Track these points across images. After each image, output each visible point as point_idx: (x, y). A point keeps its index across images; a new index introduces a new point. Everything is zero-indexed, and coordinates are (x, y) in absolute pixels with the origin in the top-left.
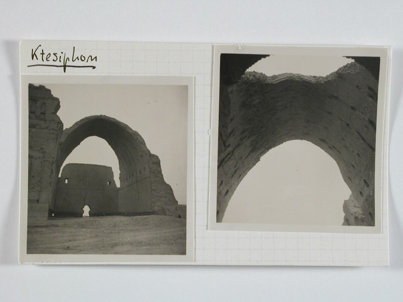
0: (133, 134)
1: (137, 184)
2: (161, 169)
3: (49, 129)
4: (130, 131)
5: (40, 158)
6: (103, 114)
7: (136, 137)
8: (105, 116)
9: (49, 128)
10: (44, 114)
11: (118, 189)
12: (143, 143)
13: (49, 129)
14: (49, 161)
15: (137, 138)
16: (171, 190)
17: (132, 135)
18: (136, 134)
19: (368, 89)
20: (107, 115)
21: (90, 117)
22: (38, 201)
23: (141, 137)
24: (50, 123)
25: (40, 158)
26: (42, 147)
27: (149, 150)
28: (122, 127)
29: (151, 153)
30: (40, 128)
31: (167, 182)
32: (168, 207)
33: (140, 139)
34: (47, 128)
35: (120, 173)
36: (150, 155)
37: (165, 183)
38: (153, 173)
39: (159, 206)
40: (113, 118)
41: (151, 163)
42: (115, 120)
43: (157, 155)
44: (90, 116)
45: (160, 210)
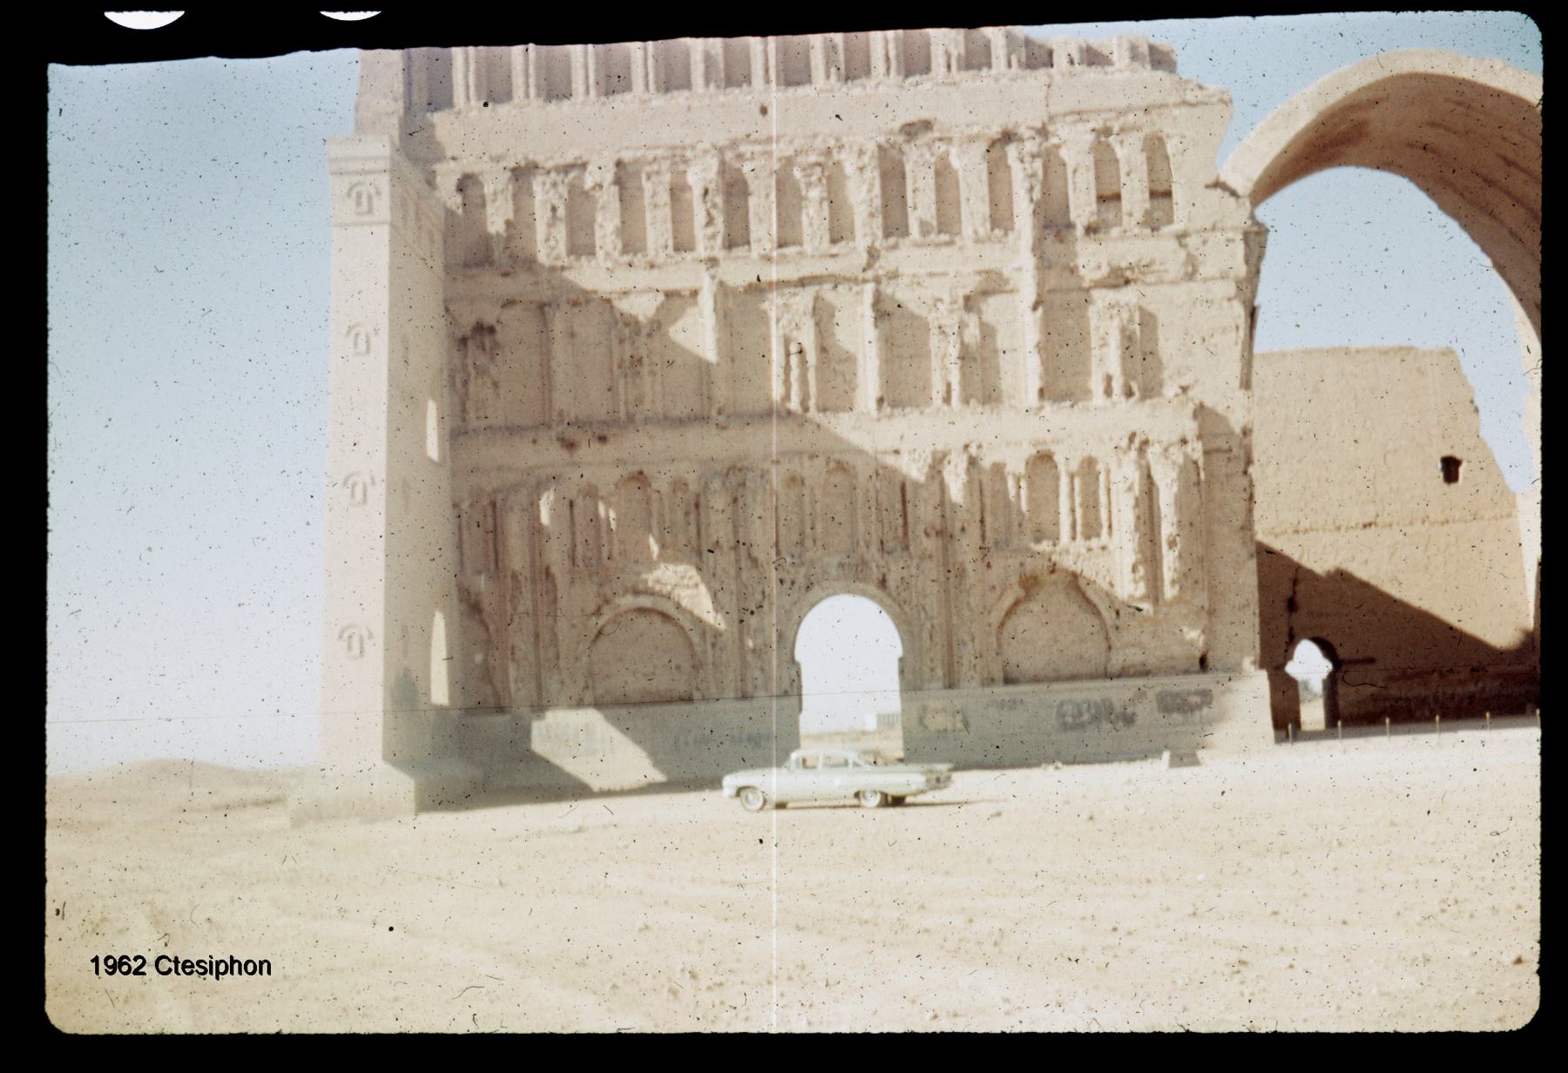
3: (1205, 280)
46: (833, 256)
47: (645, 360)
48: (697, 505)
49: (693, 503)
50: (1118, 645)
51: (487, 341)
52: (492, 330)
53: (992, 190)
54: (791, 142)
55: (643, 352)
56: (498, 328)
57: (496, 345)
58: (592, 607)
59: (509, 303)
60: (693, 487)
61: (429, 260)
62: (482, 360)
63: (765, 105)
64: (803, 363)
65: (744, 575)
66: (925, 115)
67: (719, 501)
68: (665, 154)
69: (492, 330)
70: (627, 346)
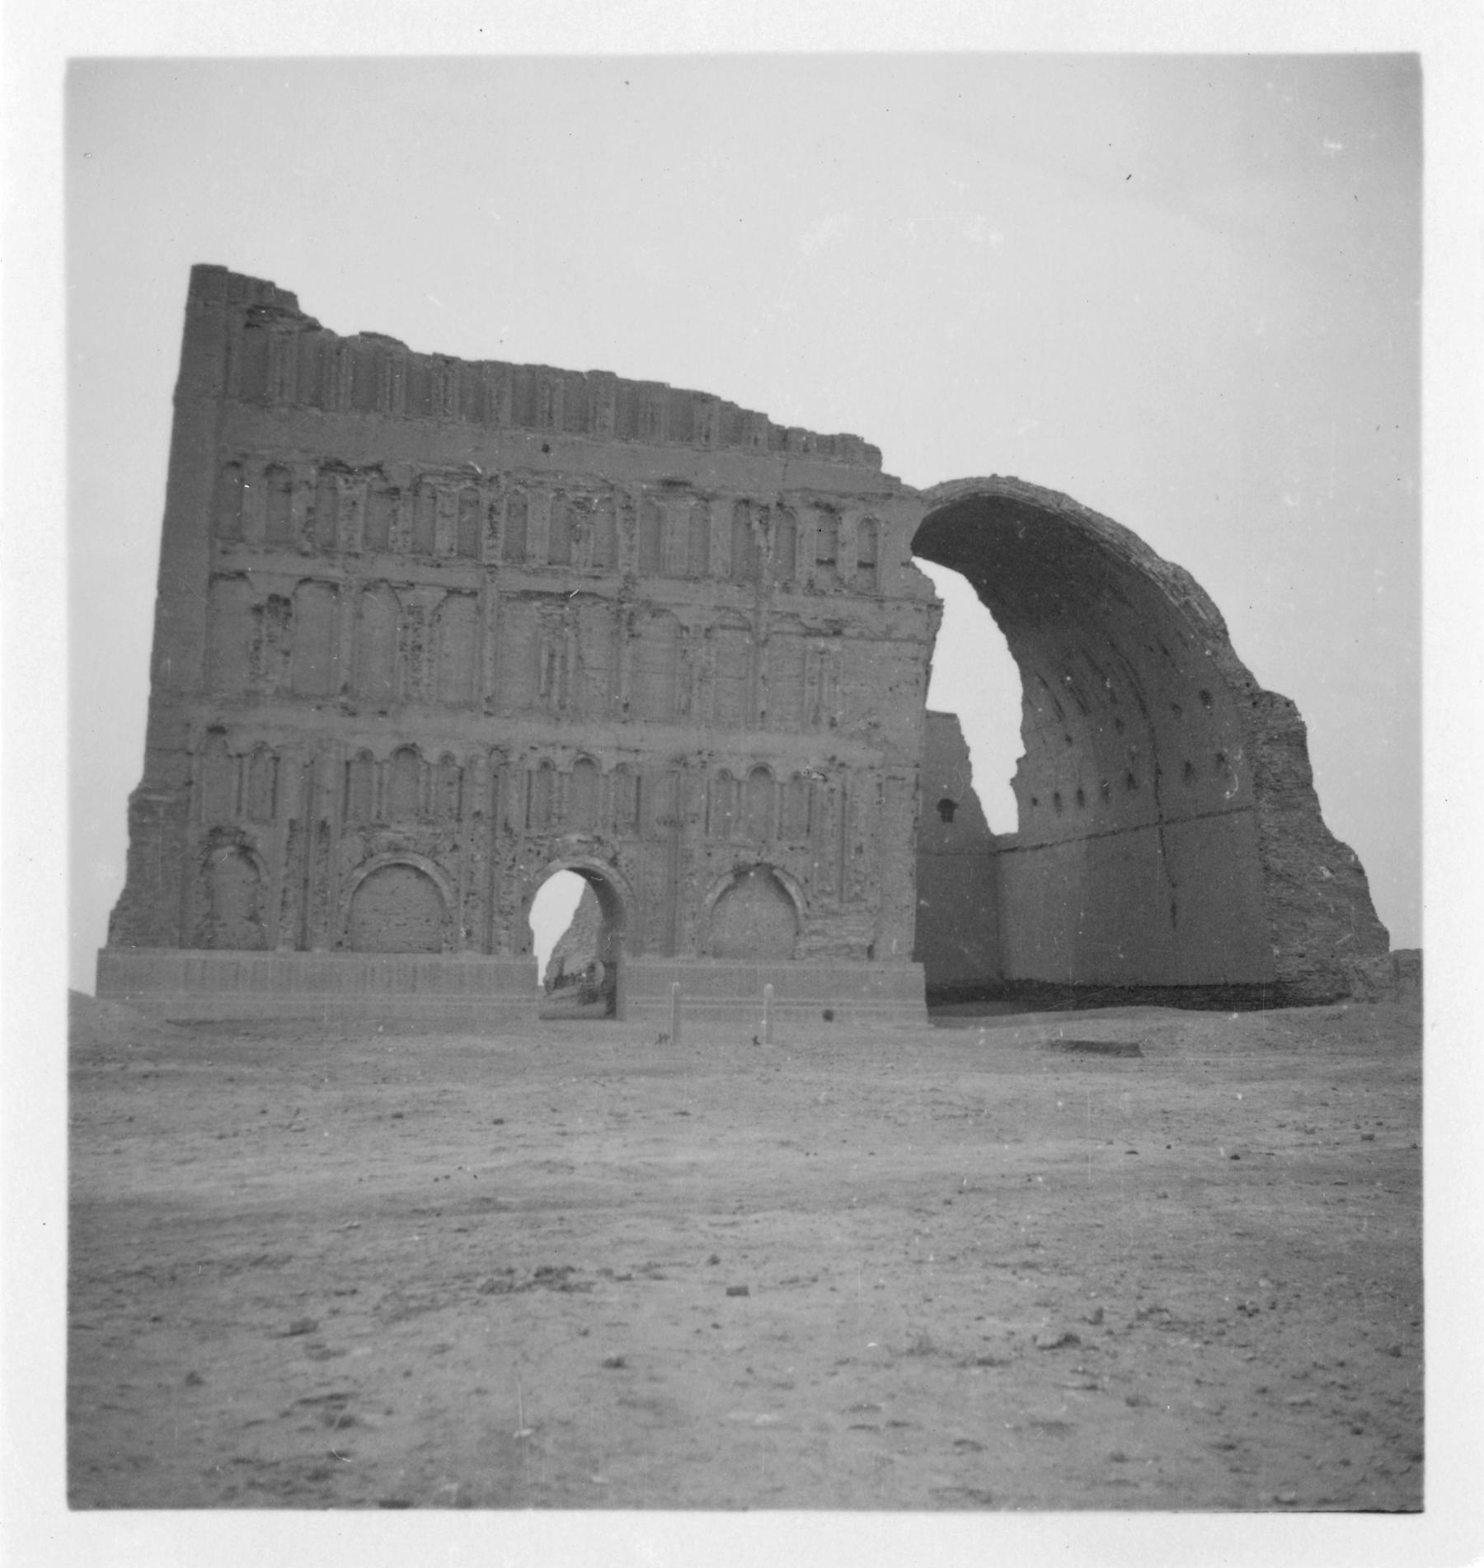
0: (1165, 583)
1: (445, 600)
2: (1309, 768)
3: (896, 640)
4: (1147, 565)
5: (872, 768)
6: (1002, 473)
7: (1183, 599)
8: (1013, 480)
9: (895, 634)
10: (872, 566)
11: (999, 848)
12: (1219, 632)
13: (896, 640)
14: (903, 779)
15: (1187, 603)
16: (1359, 871)
17: (1160, 584)
18: (1182, 582)
19: (1109, 1451)
20: (1025, 477)
21: (940, 493)
22: (870, 951)
23: (1206, 596)
24: (898, 608)
25: (872, 768)
26: (874, 719)
27: (1249, 666)
28: (1102, 541)
29: (1258, 687)
30: (861, 636)
31: (1339, 835)
32: (1357, 962)
33: (1201, 613)
34: (887, 636)
35: (1021, 752)
36: (1257, 698)
37: (1328, 836)
38: (1274, 789)
39: (1302, 956)
40: (1055, 493)
41: (1262, 736)
42: (1065, 506)
43: (1290, 696)
44: (942, 485)
45: (1309, 973)
46: (596, 578)
47: (425, 647)
48: (461, 778)
49: (457, 776)
50: (806, 931)
51: (283, 610)
52: (287, 602)
53: (564, 1018)
54: (1177, 1390)
55: (423, 641)
56: (293, 602)
57: (289, 615)
58: (358, 860)
59: (307, 580)
60: (459, 762)
61: (549, 618)
62: (277, 630)
63: (548, 443)
64: (564, 667)
65: (498, 843)
66: (729, 1299)
67: (481, 776)
68: (1287, 1145)
69: (287, 602)
70: (410, 632)
